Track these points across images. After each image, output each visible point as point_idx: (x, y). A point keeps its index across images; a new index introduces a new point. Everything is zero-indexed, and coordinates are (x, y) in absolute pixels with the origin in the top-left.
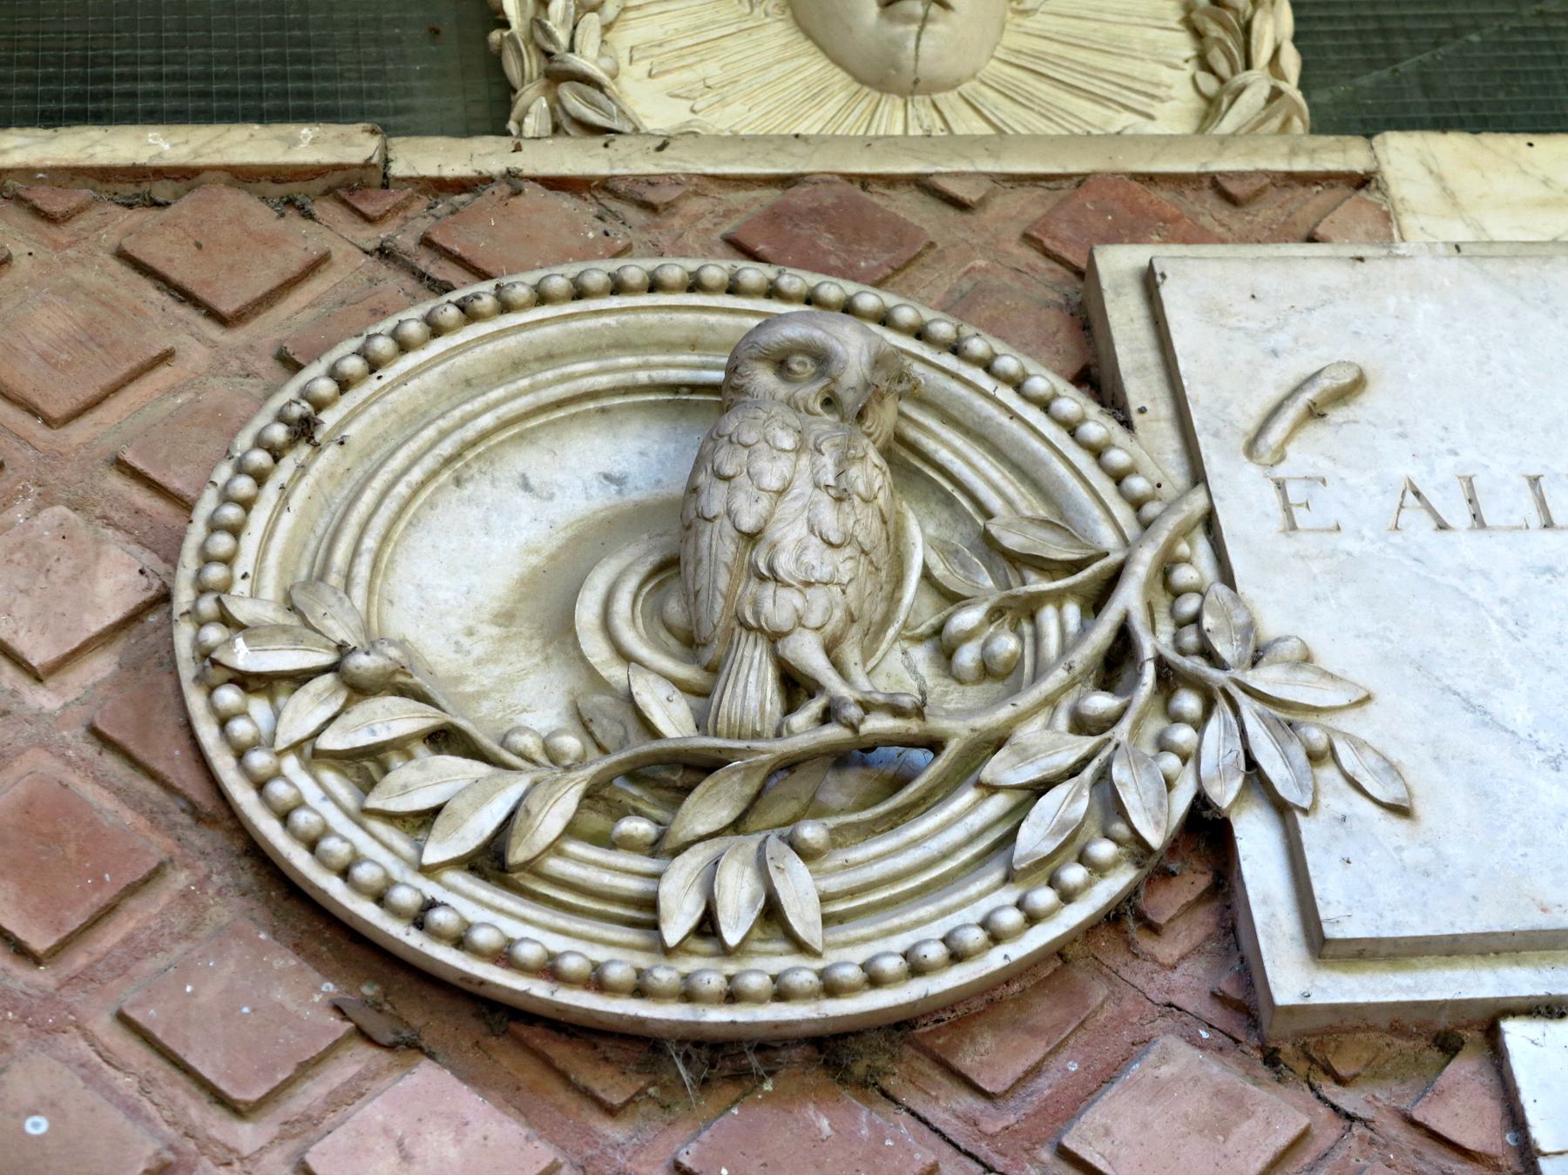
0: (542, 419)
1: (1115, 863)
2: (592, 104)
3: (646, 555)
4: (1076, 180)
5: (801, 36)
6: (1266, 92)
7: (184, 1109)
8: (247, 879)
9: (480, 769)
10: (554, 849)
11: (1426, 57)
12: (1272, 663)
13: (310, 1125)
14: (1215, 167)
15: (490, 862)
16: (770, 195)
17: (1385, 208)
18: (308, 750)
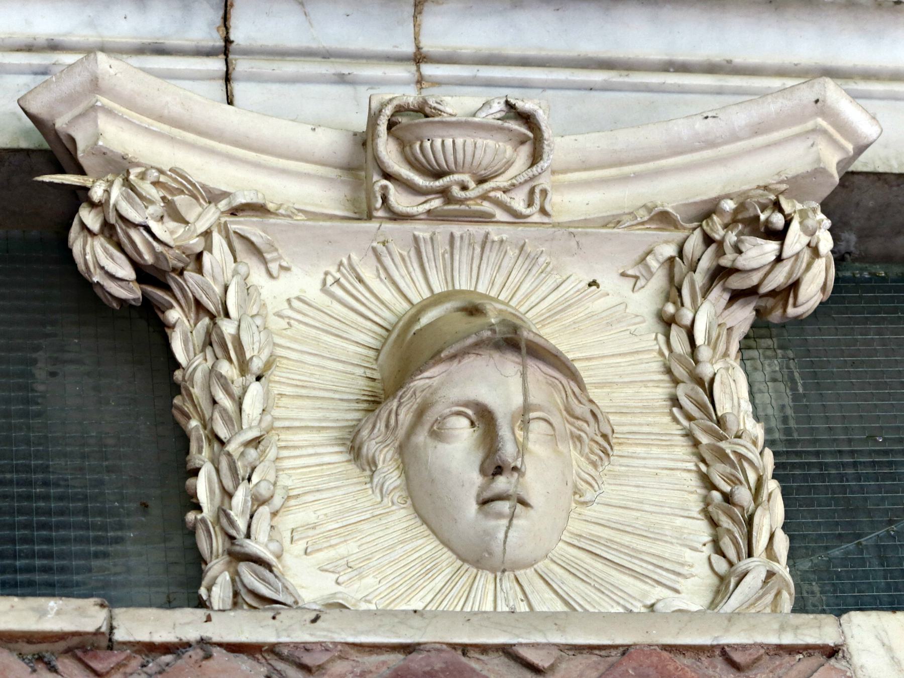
2: (264, 580)
4: (621, 649)
5: (418, 521)
6: (763, 576)
11: (881, 532)
14: (724, 641)
16: (395, 659)
17: (848, 674)
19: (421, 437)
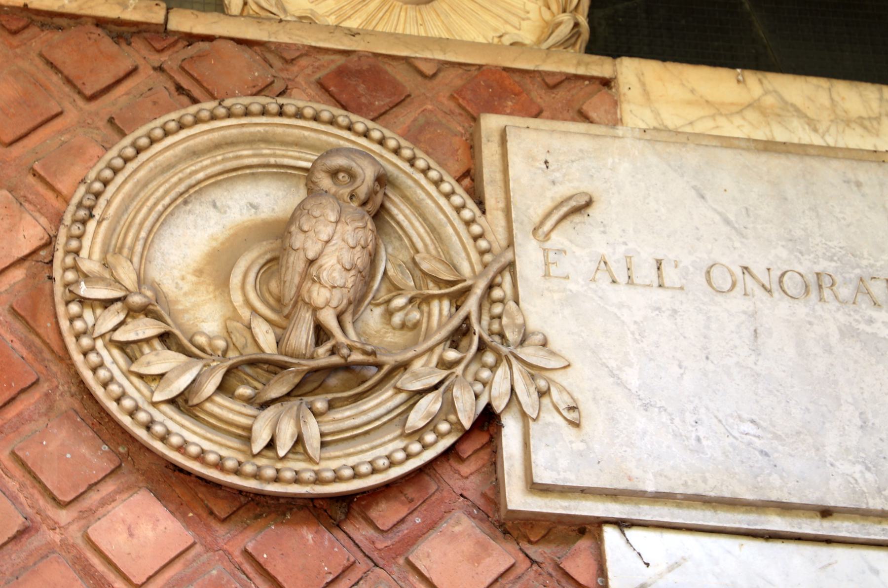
0: (226, 176)
1: (449, 433)
3: (265, 253)
7: (37, 500)
8: (74, 389)
9: (182, 358)
10: (209, 399)
12: (529, 346)
13: (90, 515)
15: (182, 403)
16: (340, 60)
18: (107, 337)
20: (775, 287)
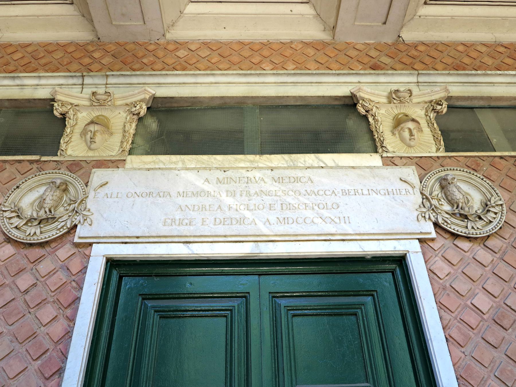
19: (401, 132)
20: (140, 195)
